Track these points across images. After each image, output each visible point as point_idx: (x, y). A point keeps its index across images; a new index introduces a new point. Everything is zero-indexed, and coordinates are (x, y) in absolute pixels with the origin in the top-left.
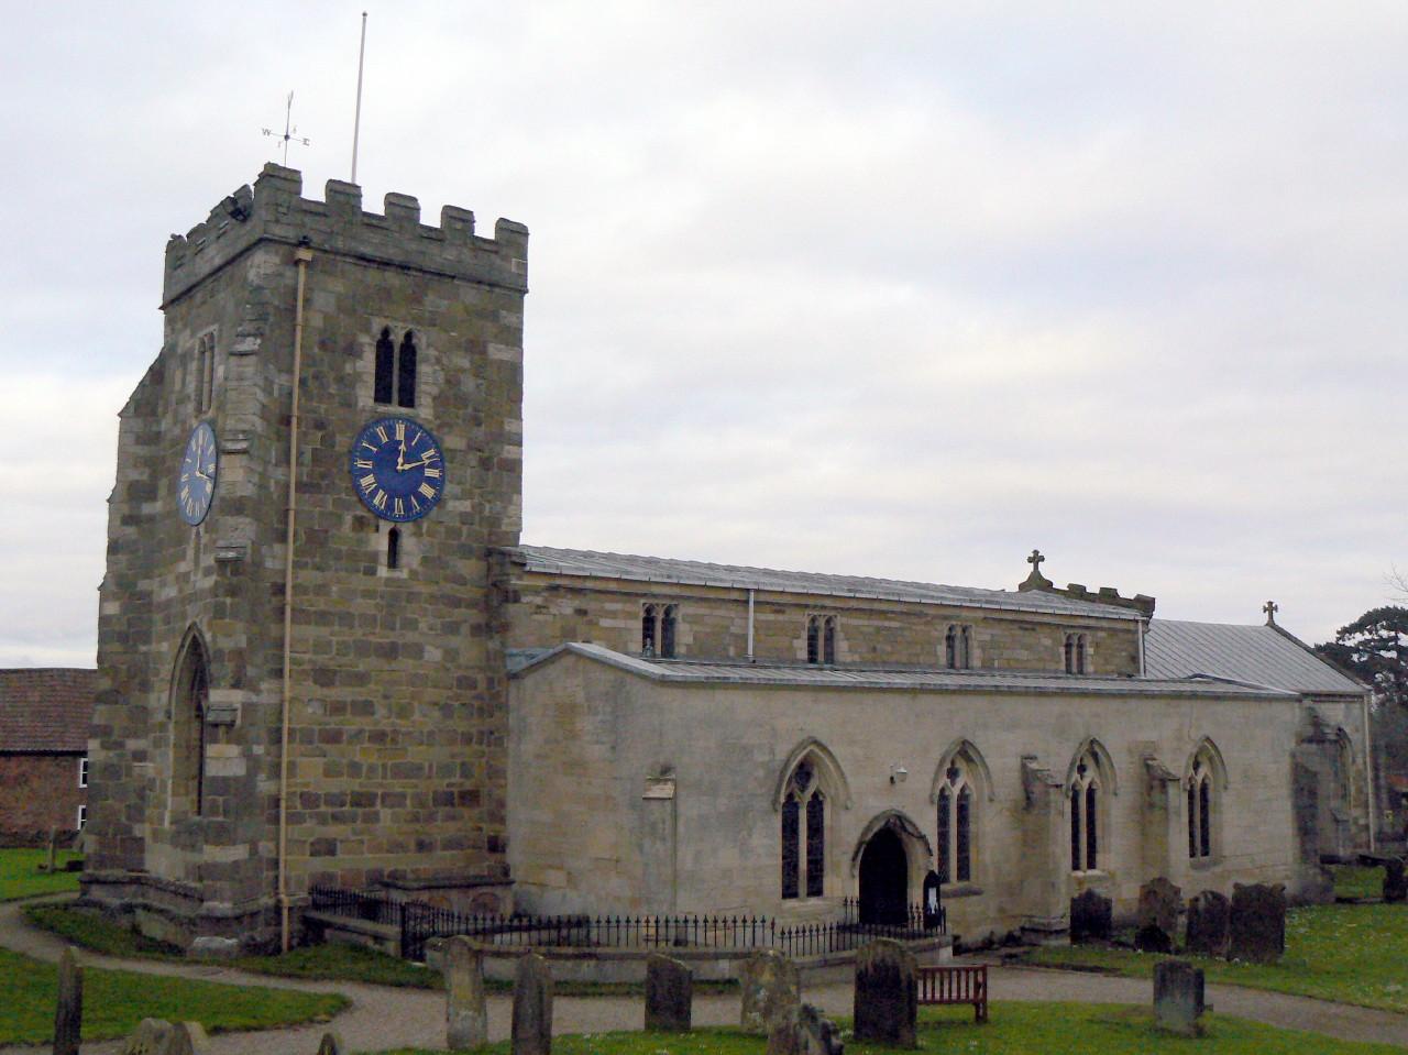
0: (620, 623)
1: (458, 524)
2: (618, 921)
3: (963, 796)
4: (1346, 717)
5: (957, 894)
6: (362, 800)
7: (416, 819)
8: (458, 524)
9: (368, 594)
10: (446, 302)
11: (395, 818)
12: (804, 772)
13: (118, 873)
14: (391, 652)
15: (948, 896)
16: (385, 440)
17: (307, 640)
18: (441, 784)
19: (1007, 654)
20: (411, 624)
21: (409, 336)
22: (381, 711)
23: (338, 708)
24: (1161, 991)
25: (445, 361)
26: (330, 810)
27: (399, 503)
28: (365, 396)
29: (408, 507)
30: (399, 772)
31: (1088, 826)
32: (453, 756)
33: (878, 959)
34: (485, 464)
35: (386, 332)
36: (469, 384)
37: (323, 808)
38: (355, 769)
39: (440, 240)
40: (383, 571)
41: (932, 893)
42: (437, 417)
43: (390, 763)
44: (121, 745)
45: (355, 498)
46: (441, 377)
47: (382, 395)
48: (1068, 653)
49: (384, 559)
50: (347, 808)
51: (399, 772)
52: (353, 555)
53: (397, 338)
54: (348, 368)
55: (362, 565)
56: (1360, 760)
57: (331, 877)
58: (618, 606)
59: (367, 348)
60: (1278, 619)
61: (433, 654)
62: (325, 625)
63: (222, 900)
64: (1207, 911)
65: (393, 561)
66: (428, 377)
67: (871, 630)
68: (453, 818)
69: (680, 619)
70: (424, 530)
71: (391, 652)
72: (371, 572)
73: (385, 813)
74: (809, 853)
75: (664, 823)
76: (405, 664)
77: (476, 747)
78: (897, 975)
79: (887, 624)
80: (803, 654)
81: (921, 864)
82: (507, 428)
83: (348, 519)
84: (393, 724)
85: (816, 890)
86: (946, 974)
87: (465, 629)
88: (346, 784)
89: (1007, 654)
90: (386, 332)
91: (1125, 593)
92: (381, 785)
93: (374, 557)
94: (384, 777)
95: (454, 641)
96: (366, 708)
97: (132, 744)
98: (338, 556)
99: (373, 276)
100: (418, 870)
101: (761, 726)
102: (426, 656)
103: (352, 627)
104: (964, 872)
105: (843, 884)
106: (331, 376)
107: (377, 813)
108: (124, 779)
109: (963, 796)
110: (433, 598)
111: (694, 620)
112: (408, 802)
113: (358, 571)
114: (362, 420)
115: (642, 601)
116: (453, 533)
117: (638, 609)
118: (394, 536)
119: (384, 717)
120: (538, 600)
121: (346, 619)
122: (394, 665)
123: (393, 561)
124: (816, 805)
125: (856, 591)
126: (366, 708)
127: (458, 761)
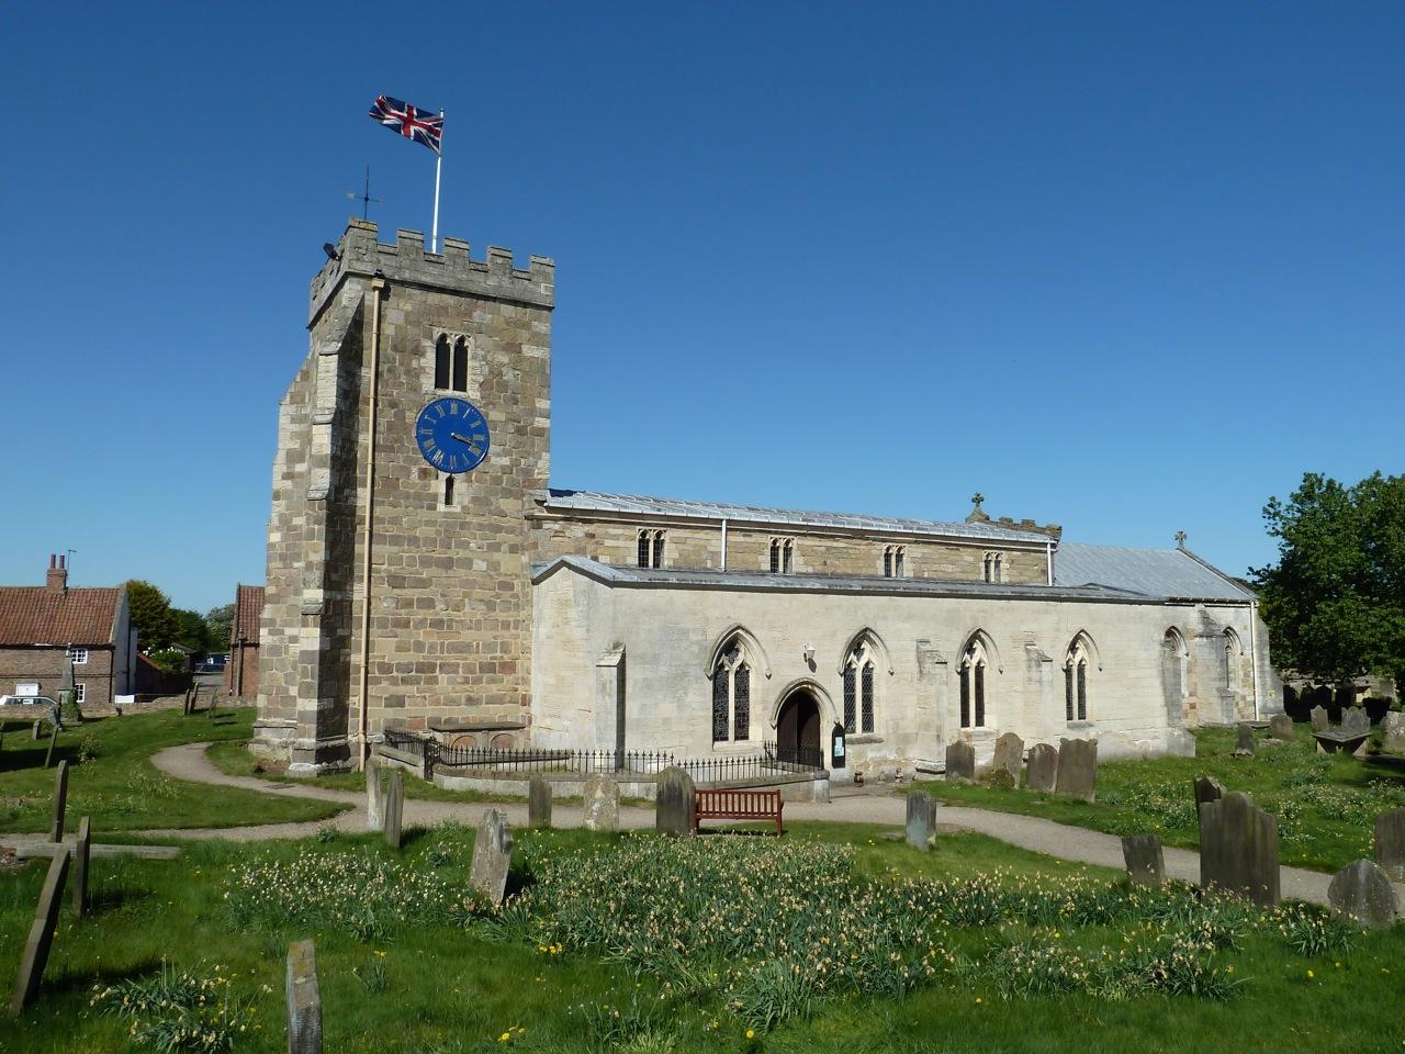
0: (621, 543)
1: (500, 474)
2: (580, 754)
3: (867, 669)
4: (1236, 619)
5: (859, 741)
6: (423, 668)
7: (466, 681)
8: (500, 474)
9: (428, 523)
10: (490, 316)
11: (450, 681)
12: (730, 646)
13: (279, 721)
14: (448, 564)
15: (852, 742)
16: (442, 414)
17: (384, 556)
18: (487, 657)
19: (935, 567)
20: (465, 545)
21: (462, 340)
22: (440, 606)
23: (408, 604)
24: (910, 814)
25: (489, 358)
26: (400, 675)
27: (453, 459)
28: (428, 382)
29: (460, 461)
30: (454, 648)
31: (976, 694)
32: (495, 637)
33: (670, 780)
34: (520, 431)
35: (443, 337)
36: (509, 375)
37: (395, 674)
38: (419, 647)
39: (485, 272)
40: (441, 507)
41: (839, 740)
42: (482, 398)
43: (446, 642)
44: (282, 632)
45: (421, 456)
46: (486, 369)
47: (441, 382)
48: (987, 567)
49: (443, 499)
50: (413, 673)
51: (454, 648)
52: (418, 496)
53: (451, 341)
54: (414, 364)
55: (425, 503)
56: (1247, 652)
57: (401, 722)
58: (620, 531)
59: (429, 350)
60: (985, 508)
61: (480, 565)
62: (396, 545)
63: (309, 737)
64: (1040, 758)
65: (448, 501)
66: (475, 370)
67: (824, 549)
68: (493, 681)
69: (667, 541)
70: (473, 478)
71: (448, 564)
72: (434, 508)
73: (443, 678)
74: (736, 708)
75: (611, 682)
76: (461, 572)
77: (513, 631)
78: (681, 794)
79: (835, 544)
80: (767, 566)
81: (831, 713)
82: (538, 405)
83: (415, 470)
84: (448, 615)
85: (742, 733)
86: (762, 797)
87: (504, 547)
88: (412, 657)
89: (935, 567)
90: (443, 337)
91: (1040, 524)
92: (439, 658)
93: (435, 497)
94: (442, 652)
95: (496, 556)
96: (428, 603)
97: (289, 631)
98: (407, 496)
99: (434, 298)
100: (468, 718)
101: (694, 614)
102: (475, 567)
103: (418, 547)
104: (868, 724)
105: (763, 731)
106: (402, 369)
107: (436, 677)
108: (284, 656)
109: (867, 669)
110: (481, 527)
111: (675, 541)
112: (460, 670)
113: (422, 507)
114: (427, 401)
115: (638, 527)
116: (497, 481)
117: (636, 532)
118: (450, 482)
119: (442, 610)
120: (557, 526)
121: (413, 541)
122: (451, 573)
123: (448, 501)
124: (742, 673)
125: (809, 521)
126: (428, 603)
127: (499, 641)
